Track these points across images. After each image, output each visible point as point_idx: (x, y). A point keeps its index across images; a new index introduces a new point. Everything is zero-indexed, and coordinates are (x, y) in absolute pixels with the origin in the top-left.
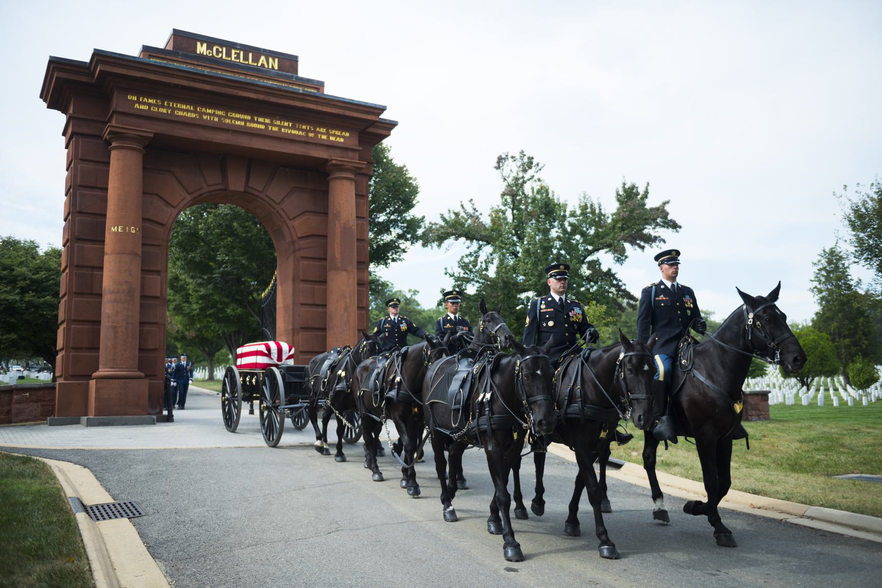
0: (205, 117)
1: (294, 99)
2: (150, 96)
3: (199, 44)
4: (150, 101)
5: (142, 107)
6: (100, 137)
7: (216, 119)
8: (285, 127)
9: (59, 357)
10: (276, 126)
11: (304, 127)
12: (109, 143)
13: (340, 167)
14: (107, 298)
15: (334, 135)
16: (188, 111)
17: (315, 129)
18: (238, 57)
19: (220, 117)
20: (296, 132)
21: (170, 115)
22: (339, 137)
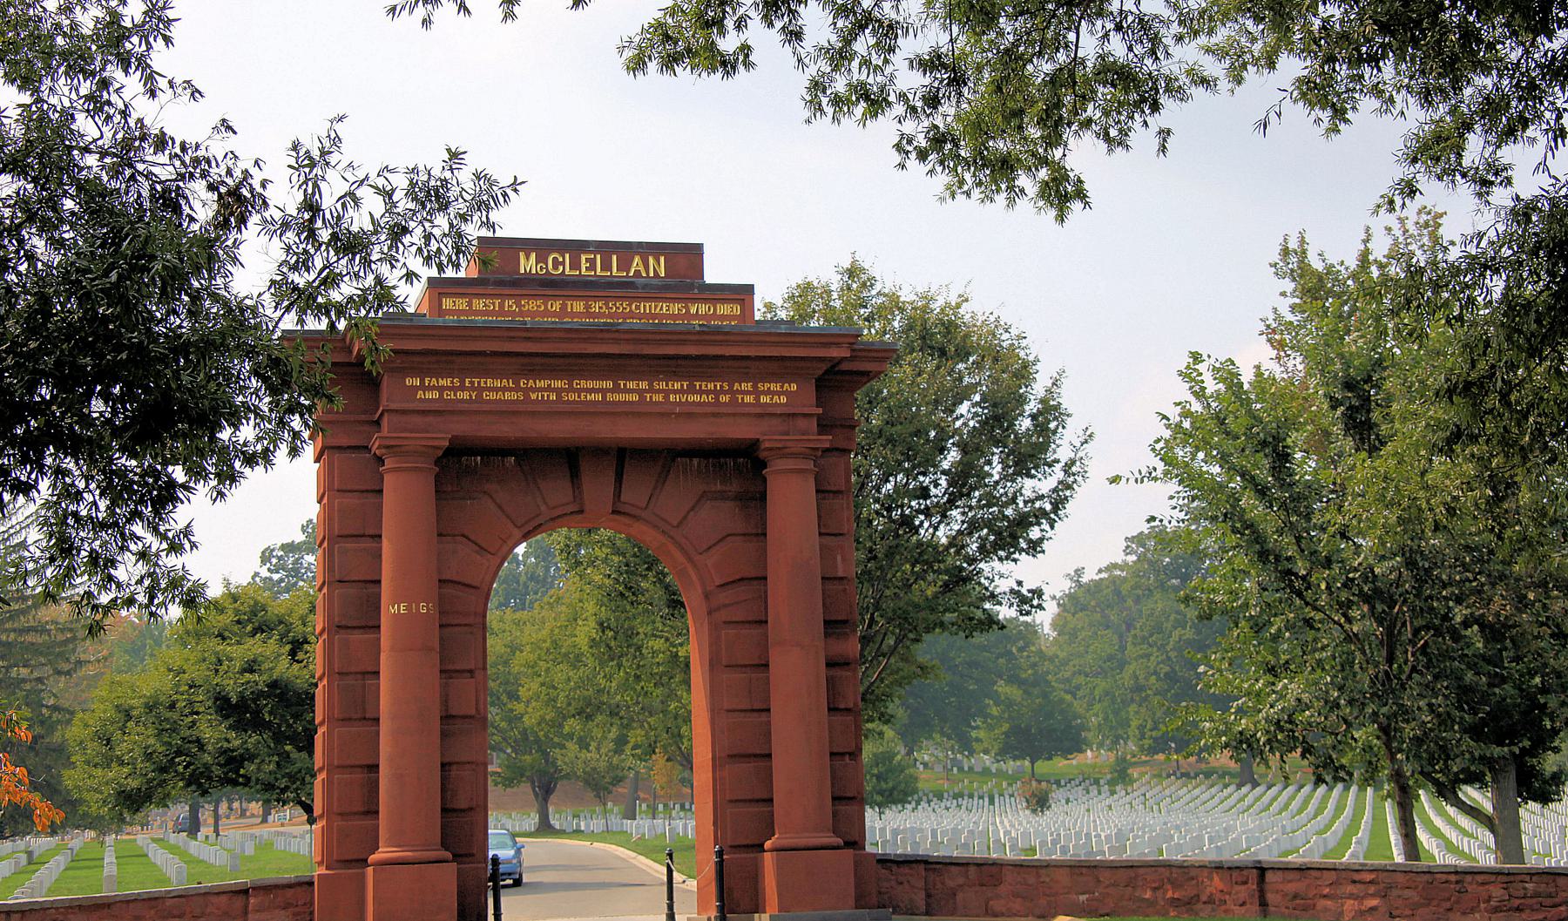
0: (533, 396)
1: (683, 342)
2: (438, 375)
3: (522, 255)
4: (442, 382)
5: (429, 395)
6: (366, 448)
7: (553, 397)
8: (675, 392)
9: (318, 738)
10: (659, 391)
11: (711, 386)
12: (380, 460)
13: (782, 453)
14: (385, 727)
15: (768, 392)
16: (504, 389)
17: (731, 386)
18: (592, 267)
19: (559, 391)
20: (696, 398)
21: (476, 401)
22: (777, 394)
